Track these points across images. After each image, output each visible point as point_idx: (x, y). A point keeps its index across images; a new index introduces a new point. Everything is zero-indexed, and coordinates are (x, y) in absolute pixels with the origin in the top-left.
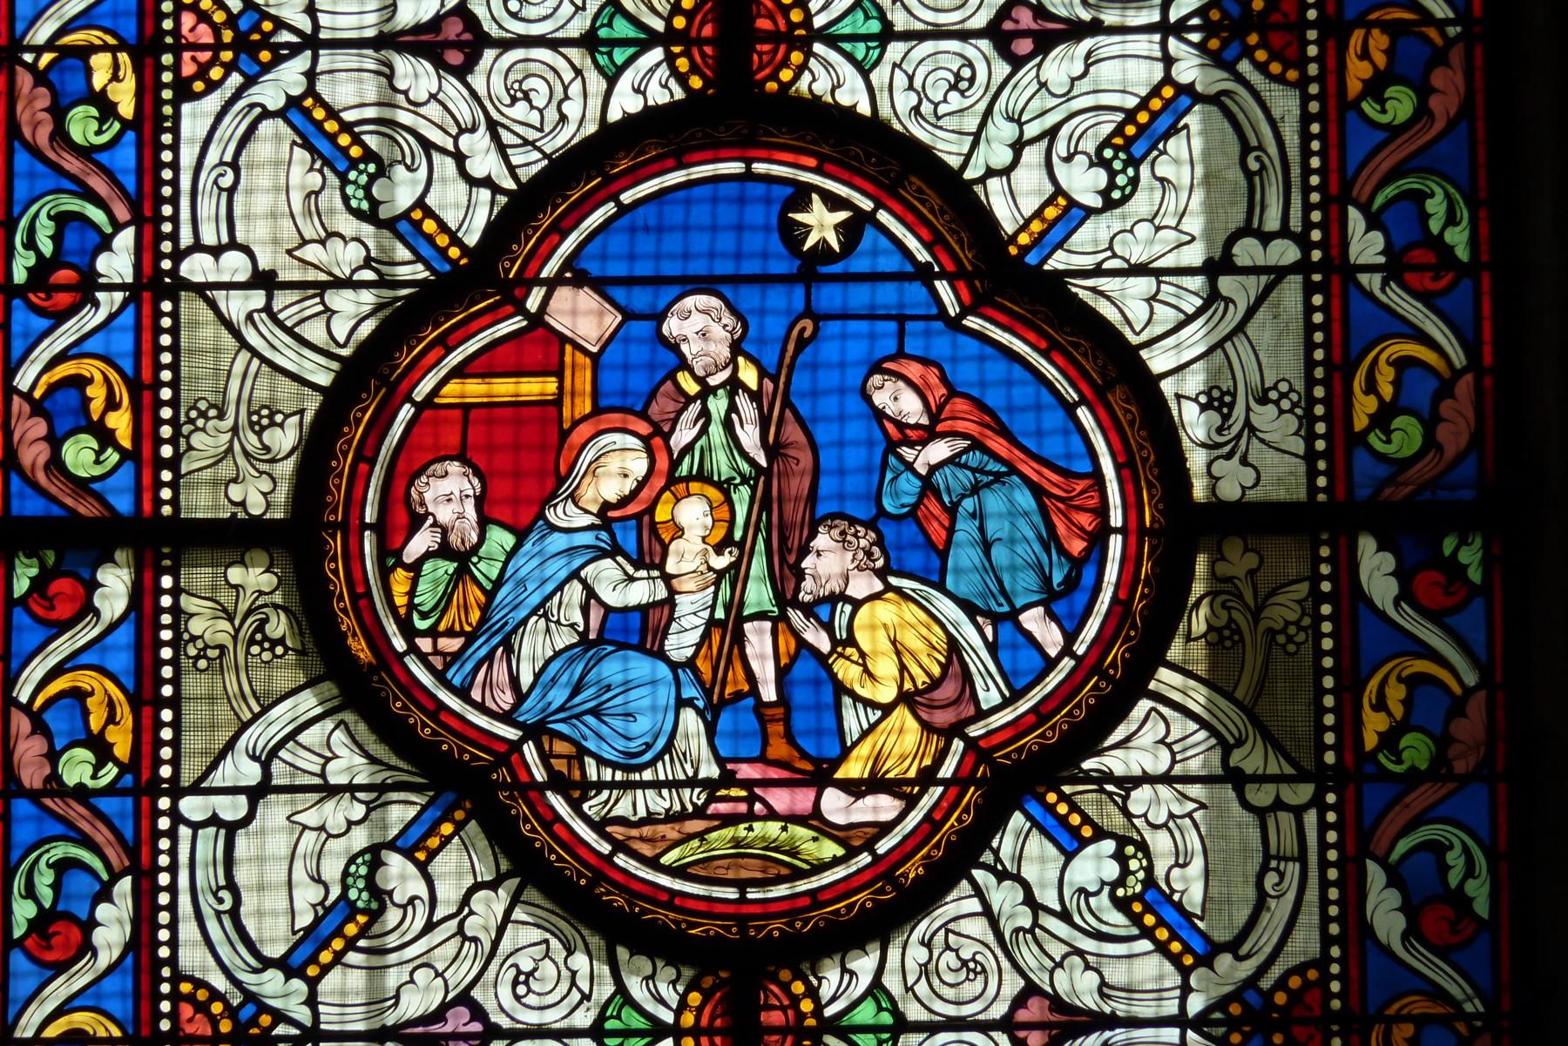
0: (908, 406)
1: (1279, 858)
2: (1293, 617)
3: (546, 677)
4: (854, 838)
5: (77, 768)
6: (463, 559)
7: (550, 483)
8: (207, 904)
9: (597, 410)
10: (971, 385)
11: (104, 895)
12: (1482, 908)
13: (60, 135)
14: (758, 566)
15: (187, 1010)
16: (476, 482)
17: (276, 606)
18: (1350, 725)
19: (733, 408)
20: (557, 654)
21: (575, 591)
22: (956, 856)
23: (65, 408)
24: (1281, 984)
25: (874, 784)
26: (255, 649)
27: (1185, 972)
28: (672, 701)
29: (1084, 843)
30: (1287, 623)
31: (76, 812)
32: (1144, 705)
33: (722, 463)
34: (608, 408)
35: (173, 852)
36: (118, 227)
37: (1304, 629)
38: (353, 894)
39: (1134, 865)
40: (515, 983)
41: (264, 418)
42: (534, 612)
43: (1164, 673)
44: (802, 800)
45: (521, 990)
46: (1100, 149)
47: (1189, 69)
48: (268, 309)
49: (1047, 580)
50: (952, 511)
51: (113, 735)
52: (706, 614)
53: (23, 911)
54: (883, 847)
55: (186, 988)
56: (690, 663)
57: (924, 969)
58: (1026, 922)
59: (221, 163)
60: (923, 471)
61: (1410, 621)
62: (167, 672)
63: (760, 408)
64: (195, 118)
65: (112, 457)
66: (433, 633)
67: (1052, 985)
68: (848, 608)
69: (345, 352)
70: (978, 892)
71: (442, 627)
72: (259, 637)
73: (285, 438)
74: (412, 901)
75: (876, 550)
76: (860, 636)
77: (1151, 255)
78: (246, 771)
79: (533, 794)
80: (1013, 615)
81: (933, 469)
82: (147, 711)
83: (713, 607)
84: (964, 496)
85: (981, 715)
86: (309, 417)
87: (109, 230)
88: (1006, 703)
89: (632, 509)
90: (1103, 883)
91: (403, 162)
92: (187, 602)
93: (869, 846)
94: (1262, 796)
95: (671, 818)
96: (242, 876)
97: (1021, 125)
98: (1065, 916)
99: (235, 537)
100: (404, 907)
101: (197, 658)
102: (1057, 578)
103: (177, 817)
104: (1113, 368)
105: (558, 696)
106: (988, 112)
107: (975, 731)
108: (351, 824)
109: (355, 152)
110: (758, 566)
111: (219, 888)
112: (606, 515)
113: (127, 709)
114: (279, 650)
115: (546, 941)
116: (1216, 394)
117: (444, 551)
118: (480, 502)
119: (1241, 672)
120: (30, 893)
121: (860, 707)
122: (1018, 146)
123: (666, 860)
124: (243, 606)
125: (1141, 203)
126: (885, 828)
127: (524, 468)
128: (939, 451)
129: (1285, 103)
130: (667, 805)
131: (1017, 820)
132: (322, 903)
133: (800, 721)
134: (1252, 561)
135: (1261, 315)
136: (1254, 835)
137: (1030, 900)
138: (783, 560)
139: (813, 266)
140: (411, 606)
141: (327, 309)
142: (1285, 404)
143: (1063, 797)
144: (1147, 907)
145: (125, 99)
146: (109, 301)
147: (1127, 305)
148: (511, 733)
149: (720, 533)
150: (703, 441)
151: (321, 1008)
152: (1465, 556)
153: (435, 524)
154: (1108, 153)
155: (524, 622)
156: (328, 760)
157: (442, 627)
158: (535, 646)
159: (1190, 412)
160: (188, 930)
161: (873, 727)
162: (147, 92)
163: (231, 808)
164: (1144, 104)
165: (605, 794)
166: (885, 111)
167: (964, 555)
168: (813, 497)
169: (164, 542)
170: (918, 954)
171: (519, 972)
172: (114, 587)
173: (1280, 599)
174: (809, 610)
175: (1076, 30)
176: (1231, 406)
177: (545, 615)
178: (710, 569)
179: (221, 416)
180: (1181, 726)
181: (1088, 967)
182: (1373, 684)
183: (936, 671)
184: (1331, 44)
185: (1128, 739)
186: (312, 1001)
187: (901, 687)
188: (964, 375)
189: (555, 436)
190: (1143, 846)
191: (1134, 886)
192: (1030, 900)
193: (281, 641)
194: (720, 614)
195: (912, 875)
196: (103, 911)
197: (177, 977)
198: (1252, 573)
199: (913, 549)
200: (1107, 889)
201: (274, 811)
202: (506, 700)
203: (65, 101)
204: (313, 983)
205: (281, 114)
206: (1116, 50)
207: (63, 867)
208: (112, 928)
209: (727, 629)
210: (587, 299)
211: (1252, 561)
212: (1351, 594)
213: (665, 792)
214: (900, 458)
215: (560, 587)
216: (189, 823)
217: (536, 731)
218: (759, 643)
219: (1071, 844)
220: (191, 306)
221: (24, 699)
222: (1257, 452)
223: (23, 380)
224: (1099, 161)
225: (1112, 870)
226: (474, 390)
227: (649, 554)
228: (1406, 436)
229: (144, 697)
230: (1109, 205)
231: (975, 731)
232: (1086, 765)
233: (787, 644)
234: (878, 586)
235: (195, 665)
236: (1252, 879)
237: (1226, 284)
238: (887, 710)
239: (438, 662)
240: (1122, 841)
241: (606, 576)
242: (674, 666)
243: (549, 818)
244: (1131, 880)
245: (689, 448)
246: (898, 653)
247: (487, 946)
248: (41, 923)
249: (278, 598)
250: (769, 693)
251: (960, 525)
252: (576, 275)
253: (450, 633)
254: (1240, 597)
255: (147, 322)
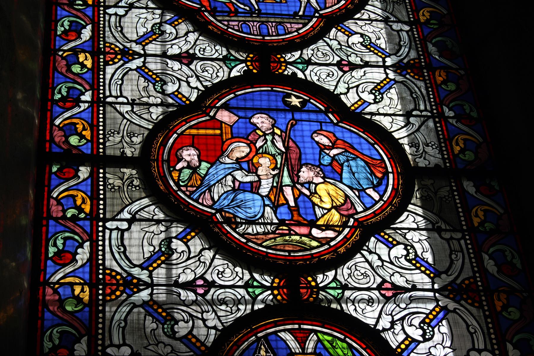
0: (325, 141)
1: (455, 251)
2: (447, 195)
3: (222, 198)
4: (322, 242)
5: (76, 69)
6: (195, 170)
7: (220, 153)
8: (115, 249)
9: (233, 137)
10: (346, 132)
11: (81, 246)
12: (519, 266)
13: (69, 70)
14: (286, 173)
15: (108, 278)
16: (197, 152)
17: (136, 178)
18: (469, 220)
19: (274, 138)
20: (225, 192)
21: (229, 178)
22: (357, 247)
23: (70, 129)
24: (463, 281)
25: (328, 227)
26: (130, 188)
27: (152, 299)
28: (262, 204)
29: (394, 246)
30: (445, 196)
31: (70, 224)
32: (406, 214)
33: (272, 150)
34: (236, 137)
35: (104, 236)
36: (87, 25)
37: (450, 197)
38: (163, 249)
39: (411, 251)
40: (218, 274)
41: (131, 135)
42: (217, 182)
43: (410, 206)
44: (304, 230)
45: (220, 276)
46: (371, 91)
47: (391, 75)
48: (132, 110)
49: (373, 183)
50: (342, 165)
51: (86, 63)
52: (271, 185)
53: (52, 250)
54: (332, 243)
55: (108, 272)
56: (267, 196)
57: (349, 275)
58: (380, 264)
59: (118, 79)
60: (332, 156)
61: (479, 196)
62: (101, 192)
63: (282, 138)
64: (110, 70)
65: (84, 141)
66: (186, 186)
67: (391, 280)
68: (314, 185)
69: (155, 121)
70: (363, 256)
71: (189, 184)
72: (131, 185)
73: (137, 140)
74: (183, 252)
75: (320, 172)
76: (318, 192)
77: (389, 112)
78: (126, 215)
79: (219, 225)
80: (364, 190)
81: (335, 155)
82: (95, 202)
83: (273, 183)
84: (344, 162)
85: (357, 213)
86: (145, 135)
87: (84, 91)
88: (364, 211)
89: (246, 159)
90: (402, 256)
91: (172, 82)
92: (108, 175)
93: (328, 243)
94: (447, 235)
95: (264, 233)
96: (126, 242)
97: (393, 317)
98: (391, 263)
99: (122, 161)
100: (180, 253)
101: (111, 189)
102: (375, 182)
103: (105, 227)
104: (383, 137)
105: (226, 202)
106: (339, 81)
107: (356, 217)
108: (161, 232)
109: (158, 79)
110: (286, 173)
111: (119, 246)
112: (238, 161)
113: (88, 200)
114: (138, 188)
115: (227, 264)
116: (413, 144)
117: (189, 167)
118: (199, 156)
119: (434, 206)
120: (55, 245)
121: (321, 209)
122: (393, 323)
123: (264, 244)
124: (126, 177)
125: (386, 101)
126: (333, 239)
127: (212, 151)
128: (334, 152)
129: (421, 84)
130: (263, 230)
131: (373, 239)
132: (153, 251)
133: (302, 211)
134: (432, 181)
135: (423, 127)
136: (447, 246)
137: (380, 258)
138: (293, 173)
139: (294, 109)
140: (179, 180)
141: (150, 112)
142: (434, 147)
143: (386, 234)
144: (417, 262)
145: (89, 64)
146: (84, 106)
147: (385, 122)
148: (213, 211)
149: (273, 166)
150: (266, 145)
151: (154, 278)
152: (493, 183)
153: (185, 161)
154: (374, 92)
155: (214, 184)
156: (154, 215)
157: (189, 184)
158: (218, 191)
159: (407, 148)
160: (108, 256)
161: (325, 214)
162: (96, 63)
163: (121, 12)
164: (430, 313)
165: (244, 226)
166: (309, 78)
167: (346, 175)
168: (300, 159)
169: (100, 161)
170: (346, 271)
171: (219, 271)
172: (84, 172)
173: (442, 190)
174: (302, 185)
175: (406, 290)
176: (419, 146)
177: (221, 183)
178: (271, 174)
179: (118, 133)
180: (419, 219)
181: (401, 276)
182: (474, 210)
183: (343, 202)
184: (431, 73)
185: (403, 221)
186: (150, 276)
187: (332, 205)
188: (339, 135)
189: (221, 143)
190: (412, 247)
191: (412, 256)
192: (380, 258)
193: (138, 186)
194: (275, 184)
195: (342, 251)
196: (80, 250)
197: (105, 269)
198: (432, 184)
199: (332, 172)
200: (404, 257)
201: (135, 227)
202: (210, 203)
203: (70, 63)
204: (151, 272)
205: (135, 70)
206: (371, 71)
207: (65, 239)
208: (83, 254)
209: (278, 189)
210: (226, 113)
211: (432, 181)
212: (463, 192)
213: (262, 226)
214: (325, 153)
215: (225, 177)
216: (108, 229)
217: (218, 211)
218: (288, 192)
219: (390, 245)
220: (109, 109)
221: (55, 196)
222: (427, 157)
223: (57, 122)
224: (371, 92)
225: (405, 252)
226: (194, 132)
227: (253, 169)
228: (469, 156)
229: (94, 197)
230: (425, 340)
231: (356, 217)
232: (392, 226)
233: (297, 192)
234: (322, 181)
235: (111, 190)
236: (448, 256)
237: (412, 120)
238: (329, 210)
239: (188, 193)
240: (406, 246)
241: (239, 175)
242: (262, 197)
243: (226, 232)
244: (410, 255)
245: (262, 147)
246: (330, 197)
247: (208, 264)
248: (58, 253)
249: (136, 176)
250: (292, 204)
251: (344, 168)
252: (226, 107)
253: (192, 186)
254: (430, 189)
255: (95, 182)
